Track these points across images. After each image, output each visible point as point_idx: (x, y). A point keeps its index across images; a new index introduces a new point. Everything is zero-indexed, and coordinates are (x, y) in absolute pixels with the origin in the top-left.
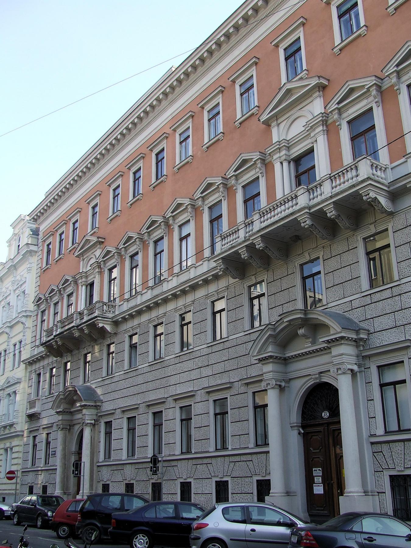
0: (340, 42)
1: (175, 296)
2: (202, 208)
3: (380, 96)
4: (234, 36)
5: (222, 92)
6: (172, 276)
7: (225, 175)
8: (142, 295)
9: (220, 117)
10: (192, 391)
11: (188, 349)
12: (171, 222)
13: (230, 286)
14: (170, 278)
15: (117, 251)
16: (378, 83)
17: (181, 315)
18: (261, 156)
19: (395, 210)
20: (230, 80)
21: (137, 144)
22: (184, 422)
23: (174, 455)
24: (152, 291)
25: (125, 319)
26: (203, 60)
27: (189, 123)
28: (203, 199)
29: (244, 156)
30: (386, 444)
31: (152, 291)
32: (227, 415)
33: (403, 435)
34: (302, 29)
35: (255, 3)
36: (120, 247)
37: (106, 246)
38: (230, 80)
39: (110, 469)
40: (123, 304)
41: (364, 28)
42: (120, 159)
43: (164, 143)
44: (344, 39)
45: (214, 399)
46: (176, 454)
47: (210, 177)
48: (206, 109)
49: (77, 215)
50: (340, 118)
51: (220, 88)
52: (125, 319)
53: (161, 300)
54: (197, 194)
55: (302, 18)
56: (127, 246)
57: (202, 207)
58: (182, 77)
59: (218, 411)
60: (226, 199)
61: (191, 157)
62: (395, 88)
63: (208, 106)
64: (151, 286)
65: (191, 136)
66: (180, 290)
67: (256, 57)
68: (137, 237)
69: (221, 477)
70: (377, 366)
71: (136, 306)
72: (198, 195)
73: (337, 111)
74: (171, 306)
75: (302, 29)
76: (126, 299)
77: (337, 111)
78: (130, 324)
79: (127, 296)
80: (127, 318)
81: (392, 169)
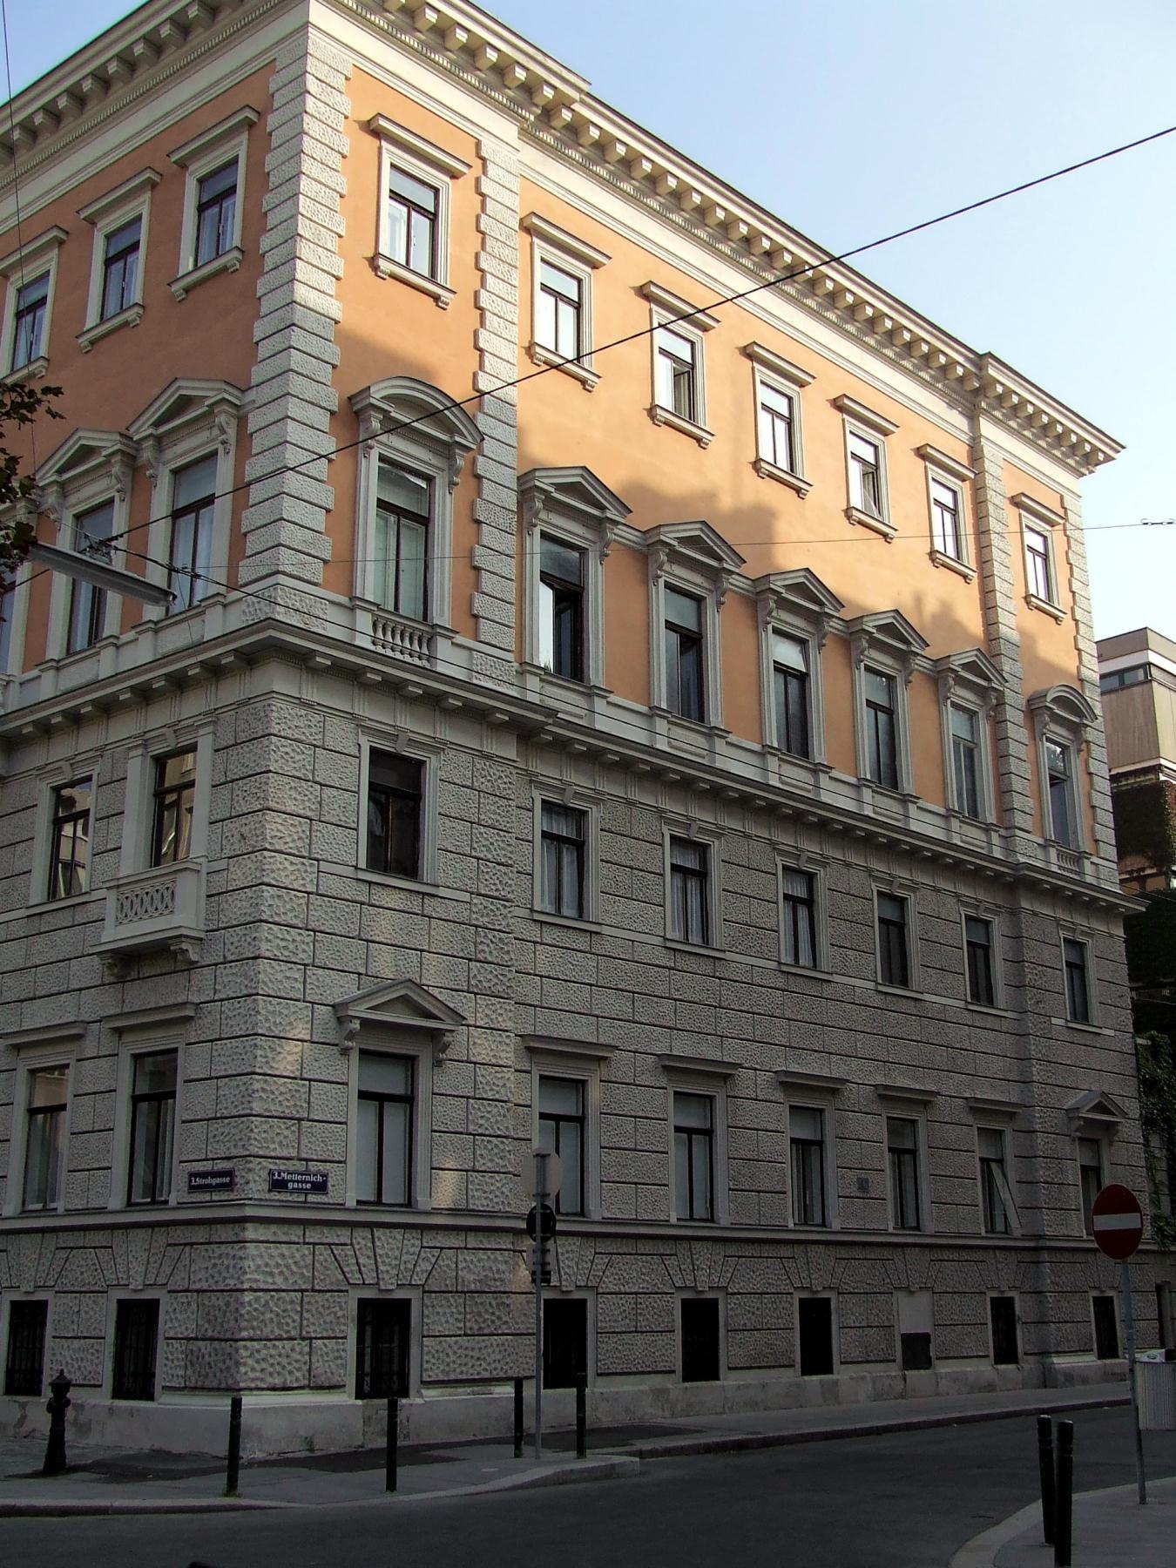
0: (191, 268)
1: (145, 696)
2: (151, 471)
3: (130, 478)
4: (201, 30)
5: (61, 243)
6: (43, 667)
7: (127, 429)
8: (225, 606)
9: (234, 204)
10: (75, 1022)
11: (69, 894)
12: (147, 454)
13: (252, 701)
14: (125, 638)
15: (124, 448)
16: (128, 450)
17: (57, 790)
18: (124, 444)
19: (7, 772)
20: (174, 158)
21: (246, 64)
22: (144, 1106)
23: (101, 1210)
24: (225, 612)
25: (46, 730)
26: (12, 149)
27: (50, 261)
28: (160, 442)
29: (85, 438)
30: (163, 1229)
31: (225, 612)
32: (170, 1101)
33: (136, 1214)
34: (244, 137)
35: (154, 28)
36: (137, 432)
37: (77, 430)
38: (173, 159)
39: (162, 1241)
40: (137, 640)
41: (236, 254)
42: (91, 159)
43: (52, 259)
44: (113, 313)
45: (133, 1052)
46: (110, 1208)
47: (90, 430)
48: (196, 170)
49: (141, 199)
50: (61, 505)
51: (148, 175)
52: (46, 730)
53: (35, 726)
54: (47, 473)
55: (149, 170)
56: (70, 480)
57: (152, 467)
58: (165, 31)
59: (143, 1089)
60: (232, 453)
61: (41, 362)
62: (148, 473)
63: (107, 220)
64: (155, 620)
65: (49, 300)
66: (63, 712)
67: (251, 107)
68: (115, 448)
69: (29, 1289)
70: (132, 1055)
71: (96, 684)
72: (143, 429)
73: (151, 442)
74: (123, 728)
75: (244, 137)
76: (150, 621)
77: (151, 442)
78: (60, 750)
79: (55, 650)
80: (84, 715)
81: (21, 684)
